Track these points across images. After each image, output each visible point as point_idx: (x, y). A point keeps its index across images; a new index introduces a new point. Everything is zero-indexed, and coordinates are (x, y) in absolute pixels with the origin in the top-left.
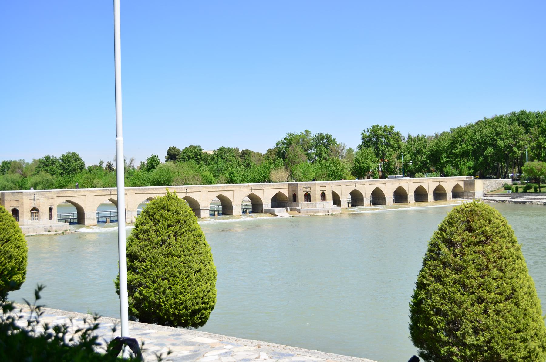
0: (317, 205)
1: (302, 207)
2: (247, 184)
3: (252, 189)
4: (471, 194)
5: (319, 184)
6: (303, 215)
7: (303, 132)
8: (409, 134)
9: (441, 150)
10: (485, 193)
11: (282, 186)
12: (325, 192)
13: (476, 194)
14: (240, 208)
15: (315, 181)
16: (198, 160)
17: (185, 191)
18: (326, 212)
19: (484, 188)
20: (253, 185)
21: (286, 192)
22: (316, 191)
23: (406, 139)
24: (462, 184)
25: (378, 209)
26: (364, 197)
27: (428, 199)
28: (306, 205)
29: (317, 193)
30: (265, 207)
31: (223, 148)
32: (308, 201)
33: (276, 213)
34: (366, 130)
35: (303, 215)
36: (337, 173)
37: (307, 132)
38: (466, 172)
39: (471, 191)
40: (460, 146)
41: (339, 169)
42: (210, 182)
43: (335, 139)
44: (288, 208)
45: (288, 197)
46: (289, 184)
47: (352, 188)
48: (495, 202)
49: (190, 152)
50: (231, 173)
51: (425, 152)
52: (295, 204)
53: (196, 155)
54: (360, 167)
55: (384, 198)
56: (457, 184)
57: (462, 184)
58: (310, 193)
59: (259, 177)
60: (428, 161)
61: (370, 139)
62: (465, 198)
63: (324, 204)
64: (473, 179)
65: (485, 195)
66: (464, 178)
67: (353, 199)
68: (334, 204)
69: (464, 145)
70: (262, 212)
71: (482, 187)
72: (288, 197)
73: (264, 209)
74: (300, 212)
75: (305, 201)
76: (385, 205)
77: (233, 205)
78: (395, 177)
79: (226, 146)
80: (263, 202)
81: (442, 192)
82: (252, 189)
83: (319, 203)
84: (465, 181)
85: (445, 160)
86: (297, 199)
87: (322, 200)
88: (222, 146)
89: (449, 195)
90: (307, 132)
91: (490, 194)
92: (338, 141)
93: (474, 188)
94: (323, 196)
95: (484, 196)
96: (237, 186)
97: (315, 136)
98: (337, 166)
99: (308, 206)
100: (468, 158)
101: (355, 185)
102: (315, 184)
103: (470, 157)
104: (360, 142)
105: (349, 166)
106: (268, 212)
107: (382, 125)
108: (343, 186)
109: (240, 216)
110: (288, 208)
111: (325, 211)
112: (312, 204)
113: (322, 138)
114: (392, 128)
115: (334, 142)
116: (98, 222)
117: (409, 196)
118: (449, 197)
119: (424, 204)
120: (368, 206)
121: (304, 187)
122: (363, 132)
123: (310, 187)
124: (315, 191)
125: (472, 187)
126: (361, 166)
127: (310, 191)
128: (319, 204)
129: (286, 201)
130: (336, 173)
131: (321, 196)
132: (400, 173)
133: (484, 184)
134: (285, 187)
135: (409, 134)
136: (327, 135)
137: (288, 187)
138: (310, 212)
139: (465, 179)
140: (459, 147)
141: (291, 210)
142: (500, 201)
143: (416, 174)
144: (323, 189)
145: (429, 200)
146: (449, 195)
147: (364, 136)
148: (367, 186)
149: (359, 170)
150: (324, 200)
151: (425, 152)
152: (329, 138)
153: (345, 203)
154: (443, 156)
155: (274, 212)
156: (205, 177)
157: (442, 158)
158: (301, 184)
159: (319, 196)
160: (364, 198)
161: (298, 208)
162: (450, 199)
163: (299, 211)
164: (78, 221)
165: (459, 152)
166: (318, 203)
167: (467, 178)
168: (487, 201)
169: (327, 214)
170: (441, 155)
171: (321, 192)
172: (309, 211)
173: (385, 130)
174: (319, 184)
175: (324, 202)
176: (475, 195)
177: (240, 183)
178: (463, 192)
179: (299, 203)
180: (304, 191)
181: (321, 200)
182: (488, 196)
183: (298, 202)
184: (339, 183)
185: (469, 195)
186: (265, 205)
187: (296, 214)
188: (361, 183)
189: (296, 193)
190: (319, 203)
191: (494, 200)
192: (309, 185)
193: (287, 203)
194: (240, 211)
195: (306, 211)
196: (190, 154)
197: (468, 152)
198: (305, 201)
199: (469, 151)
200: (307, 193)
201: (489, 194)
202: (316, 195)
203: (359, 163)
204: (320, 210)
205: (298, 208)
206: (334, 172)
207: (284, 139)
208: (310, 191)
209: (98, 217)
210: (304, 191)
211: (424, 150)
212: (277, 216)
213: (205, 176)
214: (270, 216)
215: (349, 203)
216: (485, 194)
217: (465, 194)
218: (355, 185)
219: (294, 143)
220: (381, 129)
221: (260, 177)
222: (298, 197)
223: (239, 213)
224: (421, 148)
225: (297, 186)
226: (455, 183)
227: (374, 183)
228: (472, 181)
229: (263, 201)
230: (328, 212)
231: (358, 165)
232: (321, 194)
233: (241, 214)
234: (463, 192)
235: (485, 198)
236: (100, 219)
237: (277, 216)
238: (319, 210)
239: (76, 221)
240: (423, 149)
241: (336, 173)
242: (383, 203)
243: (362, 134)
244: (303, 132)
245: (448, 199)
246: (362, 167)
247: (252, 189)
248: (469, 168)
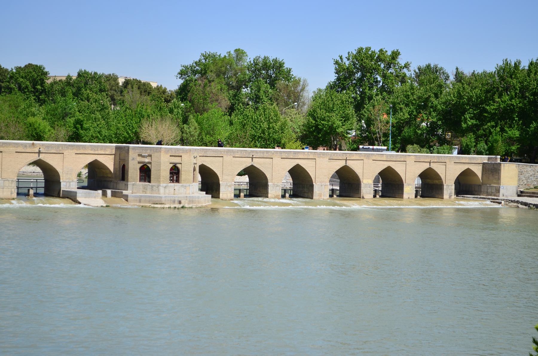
0: (162, 190)
1: (134, 191)
2: (31, 142)
3: (39, 153)
4: (494, 191)
5: (167, 151)
6: (132, 204)
7: (232, 52)
8: (457, 69)
9: (463, 104)
10: (522, 190)
11: (101, 150)
12: (178, 165)
13: (502, 191)
14: (14, 185)
15: (161, 144)
16: (37, 94)
17: (37, 151)
18: (176, 202)
19: (519, 180)
20: (43, 145)
21: (109, 163)
22: (160, 162)
23: (452, 78)
24: (478, 170)
25: (494, 205)
26: (269, 181)
27: (402, 193)
28: (141, 187)
29: (162, 167)
30: (64, 187)
31: (86, 72)
32: (145, 181)
33: (79, 199)
34: (345, 55)
35: (132, 204)
36: (269, 134)
37: (240, 53)
38: (501, 147)
39: (495, 183)
40: (499, 98)
41: (273, 128)
42: (39, 138)
43: (290, 70)
44: (109, 192)
45: (112, 171)
46: (117, 148)
47: (291, 164)
48: (527, 207)
49: (22, 77)
50: (79, 122)
51: (436, 106)
52: (123, 184)
53: (34, 83)
54: (316, 126)
55: (312, 186)
56: (468, 169)
57: (478, 170)
58: (149, 165)
59: (125, 134)
60: (440, 123)
61: (350, 73)
62: (481, 196)
63: (176, 188)
64: (499, 161)
65: (521, 194)
66: (484, 158)
67: (295, 183)
68: (202, 190)
69: (506, 98)
70: (58, 196)
71: (517, 179)
72: (112, 171)
73: (62, 189)
74: (127, 200)
75: (141, 180)
76: (312, 198)
77: (61, 181)
78: (373, 150)
79: (91, 69)
80: (61, 177)
81: (437, 182)
82: (39, 151)
83: (165, 185)
84: (484, 164)
85: (470, 123)
86: (126, 177)
87: (172, 181)
88: (83, 70)
89: (449, 188)
90: (240, 53)
91: (530, 193)
92: (295, 73)
93: (499, 179)
94: (175, 173)
95: (519, 196)
96: (10, 144)
97: (252, 62)
98: (271, 121)
99: (145, 190)
100: (512, 122)
101: (252, 158)
102: (159, 150)
103: (516, 121)
104: (332, 77)
105: (299, 124)
106: (71, 197)
107: (376, 48)
108: (228, 158)
109: (13, 199)
110: (109, 192)
111: (174, 202)
112: (152, 186)
113: (266, 66)
114: (395, 55)
115: (287, 75)
116: (18, 194)
117: (362, 185)
118: (449, 191)
119: (392, 201)
120: (276, 197)
121: (140, 155)
122: (339, 59)
123: (150, 156)
124: (159, 164)
125: (496, 177)
126: (318, 125)
127: (150, 163)
128: (165, 187)
129: (110, 178)
130: (267, 133)
131: (171, 173)
132: (384, 143)
133: (521, 173)
134: (107, 153)
135: (457, 69)
136: (275, 61)
137: (114, 153)
138: (145, 201)
139: (486, 161)
140: (497, 100)
141: (114, 195)
142: (534, 205)
143: (409, 147)
144: (176, 160)
145: (405, 196)
146: (449, 188)
147: (339, 68)
148: (277, 160)
149: (314, 131)
150: (178, 181)
151: (436, 106)
152: (278, 66)
153: (230, 189)
154: (467, 116)
155: (76, 196)
156: (30, 126)
157: (466, 119)
158: (134, 148)
159: (166, 173)
160: (270, 184)
161: (125, 192)
162: (450, 197)
163: (126, 198)
164: (45, 191)
165: (496, 109)
166: (163, 184)
167: (489, 159)
168: (515, 204)
169: (177, 206)
170: (463, 113)
171: (172, 165)
172: (143, 199)
173: (379, 59)
174: (167, 151)
175: (177, 184)
176: (499, 192)
177: (89, 142)
178: (480, 186)
179: (129, 183)
180: (139, 163)
181: (171, 180)
182: (525, 196)
183: (128, 181)
184: (220, 151)
185: (489, 190)
186: (65, 184)
187: (119, 203)
188: (266, 155)
189: (126, 166)
190: (165, 185)
191: (525, 204)
192: (149, 151)
193: (111, 181)
194: (13, 190)
195: (138, 199)
196: (21, 80)
197: (513, 111)
198: (141, 180)
199: (514, 109)
200: (145, 167)
201: (527, 193)
202: (160, 170)
203: (315, 119)
204: (163, 199)
205: (125, 192)
206: (263, 132)
207: (196, 63)
208: (150, 163)
209: (18, 188)
210: (139, 163)
211: (436, 102)
212: (80, 203)
213: (30, 124)
214: (71, 204)
215: (285, 191)
216: (522, 192)
217: (482, 190)
218: (252, 158)
219: (211, 71)
220: (371, 57)
221: (128, 133)
222: (128, 171)
223: (11, 193)
224: (430, 96)
225: (128, 153)
226: (464, 167)
227: (291, 157)
228: (495, 166)
229: (61, 174)
230: (180, 202)
231: (314, 122)
232: (172, 169)
233: (15, 195)
234: (480, 185)
235: (521, 199)
236: (21, 191)
237: (80, 203)
238: (161, 197)
239: (42, 191)
240: (433, 99)
241: (267, 133)
242: (310, 194)
243: (336, 63)
244: (232, 52)
245: (446, 196)
246: (320, 127)
247: (39, 153)
248: (510, 141)
